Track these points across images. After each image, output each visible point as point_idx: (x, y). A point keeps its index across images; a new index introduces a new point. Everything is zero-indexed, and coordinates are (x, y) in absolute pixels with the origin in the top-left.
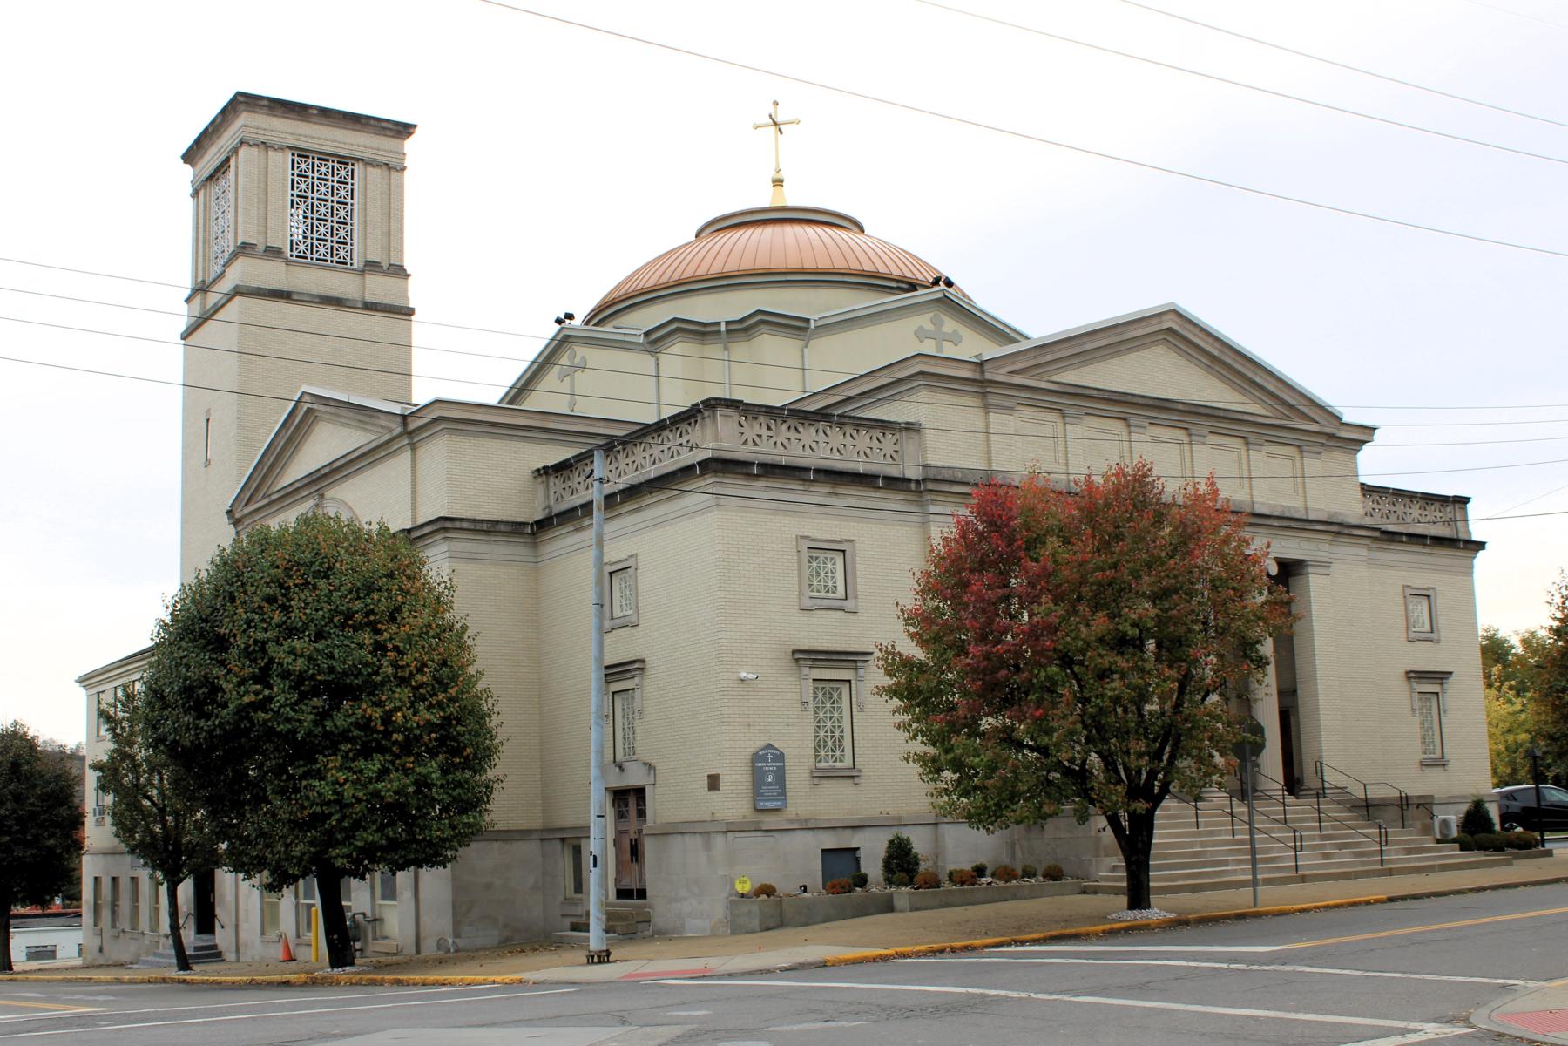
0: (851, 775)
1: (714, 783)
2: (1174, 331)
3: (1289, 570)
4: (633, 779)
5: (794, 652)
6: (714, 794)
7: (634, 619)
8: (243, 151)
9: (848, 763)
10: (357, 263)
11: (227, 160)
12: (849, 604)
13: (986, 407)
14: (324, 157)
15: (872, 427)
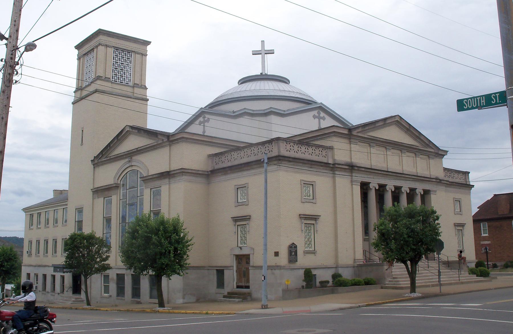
0: (314, 252)
1: (277, 254)
2: (398, 122)
3: (426, 192)
4: (245, 252)
5: (300, 215)
6: (277, 258)
7: (247, 203)
8: (100, 47)
9: (312, 249)
10: (131, 84)
11: (93, 49)
12: (314, 201)
13: (350, 143)
14: (123, 50)
15: (320, 147)
